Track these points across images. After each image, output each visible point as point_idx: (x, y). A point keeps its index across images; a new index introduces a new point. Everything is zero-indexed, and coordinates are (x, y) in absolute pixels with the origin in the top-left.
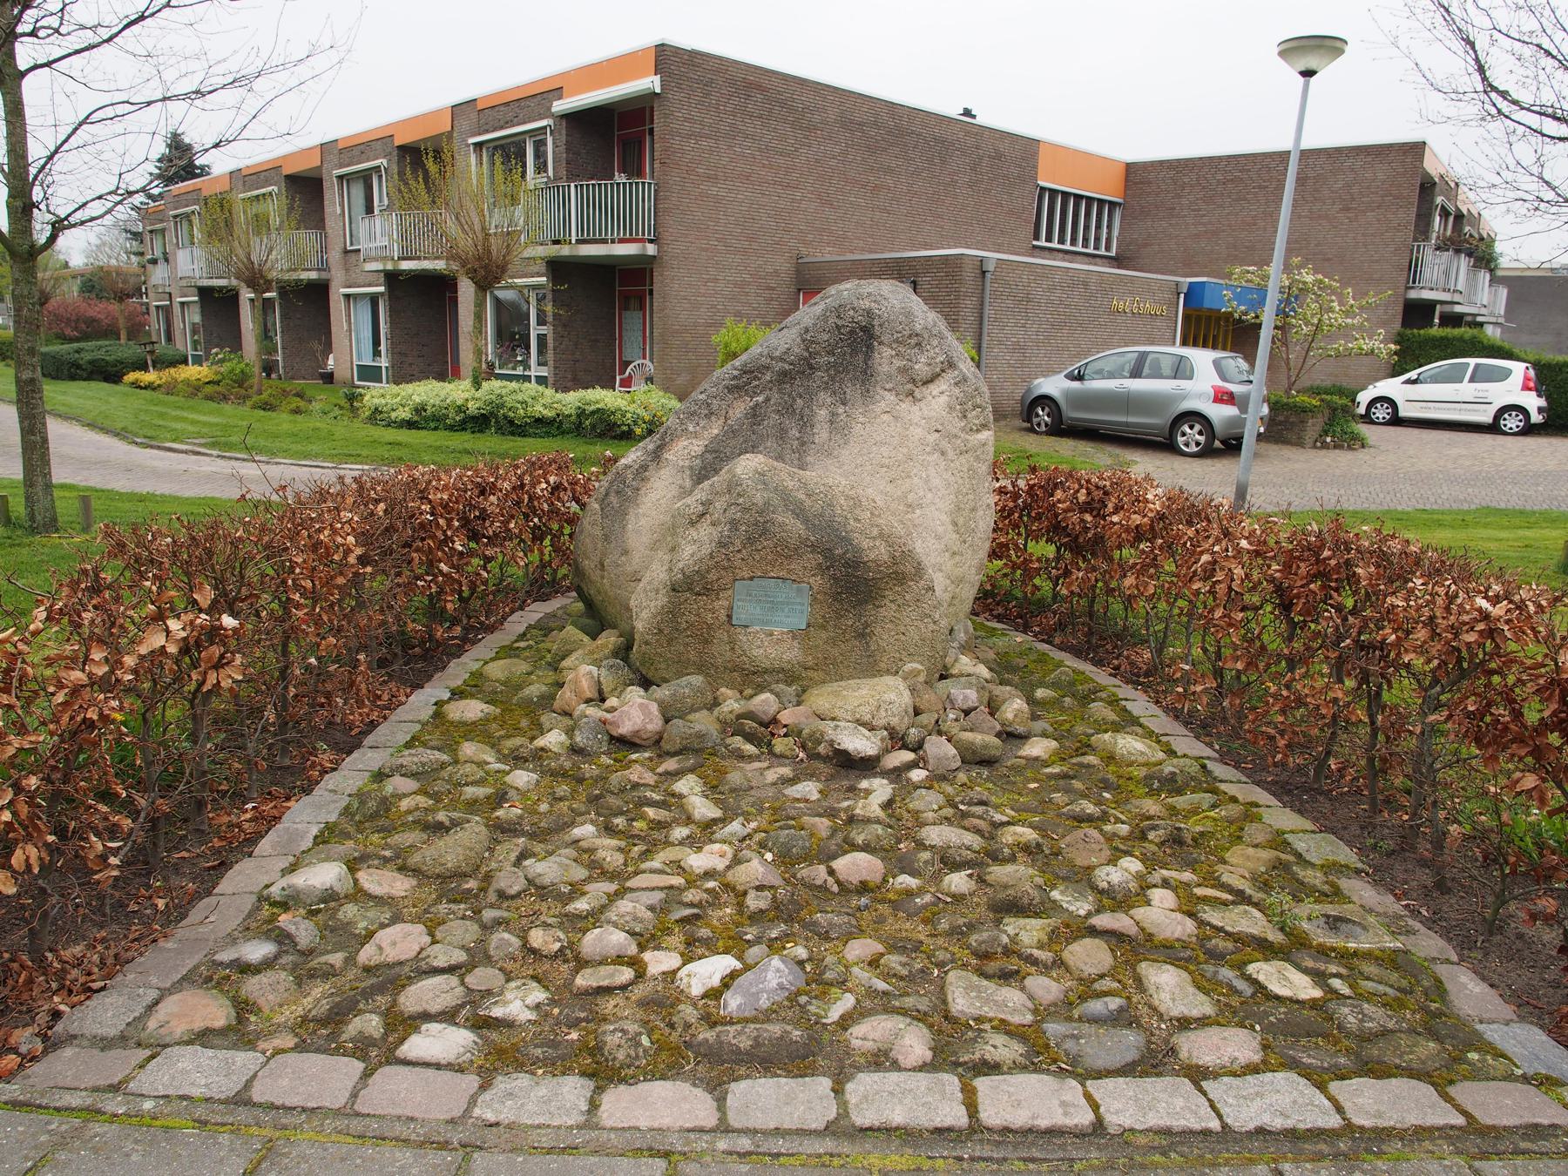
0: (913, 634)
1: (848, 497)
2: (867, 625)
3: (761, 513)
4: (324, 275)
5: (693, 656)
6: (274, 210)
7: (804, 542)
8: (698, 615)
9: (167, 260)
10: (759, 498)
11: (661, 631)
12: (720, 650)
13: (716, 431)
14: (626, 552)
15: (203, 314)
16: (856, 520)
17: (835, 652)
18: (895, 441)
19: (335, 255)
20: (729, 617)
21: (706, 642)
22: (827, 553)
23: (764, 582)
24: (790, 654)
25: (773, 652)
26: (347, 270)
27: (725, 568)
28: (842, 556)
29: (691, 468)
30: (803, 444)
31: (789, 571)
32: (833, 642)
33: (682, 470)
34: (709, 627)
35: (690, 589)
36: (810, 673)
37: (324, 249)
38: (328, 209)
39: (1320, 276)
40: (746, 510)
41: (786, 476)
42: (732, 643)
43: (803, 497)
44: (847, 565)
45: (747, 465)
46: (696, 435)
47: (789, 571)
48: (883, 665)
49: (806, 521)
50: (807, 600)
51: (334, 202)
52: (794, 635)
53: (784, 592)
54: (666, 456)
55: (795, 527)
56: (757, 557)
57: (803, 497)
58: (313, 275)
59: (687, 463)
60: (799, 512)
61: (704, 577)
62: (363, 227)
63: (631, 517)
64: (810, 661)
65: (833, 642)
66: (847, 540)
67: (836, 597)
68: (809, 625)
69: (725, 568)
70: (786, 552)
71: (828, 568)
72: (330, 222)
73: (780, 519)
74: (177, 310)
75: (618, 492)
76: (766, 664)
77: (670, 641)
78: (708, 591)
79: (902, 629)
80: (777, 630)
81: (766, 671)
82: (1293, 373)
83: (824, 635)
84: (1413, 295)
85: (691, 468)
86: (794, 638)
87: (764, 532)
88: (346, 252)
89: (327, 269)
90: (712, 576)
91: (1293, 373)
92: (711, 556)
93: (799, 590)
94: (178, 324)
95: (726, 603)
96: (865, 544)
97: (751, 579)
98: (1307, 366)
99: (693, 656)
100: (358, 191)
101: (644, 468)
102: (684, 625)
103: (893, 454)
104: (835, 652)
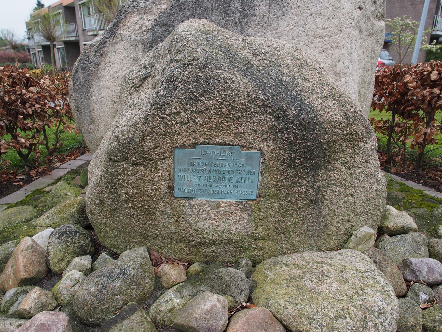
0: (361, 196)
1: (293, 58)
2: (319, 190)
3: (202, 68)
4: (77, 38)
5: (137, 226)
6: (61, 19)
7: (253, 100)
8: (137, 186)
9: (33, 38)
10: (201, 53)
11: (102, 202)
12: (164, 222)
13: (164, 7)
14: (93, 121)
15: (44, 54)
16: (306, 80)
17: (288, 221)
18: (329, 12)
19: (80, 32)
20: (171, 188)
21: (149, 214)
22: (279, 113)
23: (208, 149)
24: (239, 225)
25: (220, 225)
26: (84, 36)
27: (161, 134)
28: (296, 117)
29: (143, 41)
30: (245, 16)
31: (237, 135)
32: (285, 211)
33: (134, 43)
34: (151, 199)
35: (126, 159)
36: (261, 244)
37: (77, 31)
38: (77, 16)
39: (414, 21)
40: (185, 66)
41: (232, 38)
42: (176, 216)
43: (249, 56)
44: (302, 127)
45: (189, 27)
46: (146, 11)
47: (237, 135)
48: (332, 229)
49: (254, 79)
50: (257, 168)
51: (79, 14)
52: (243, 206)
53: (231, 159)
54: (120, 31)
55: (243, 85)
56: (199, 120)
57: (249, 56)
58: (74, 39)
59: (139, 37)
60: (246, 69)
61: (139, 145)
62: (87, 20)
63: (94, 90)
64: (261, 232)
65: (285, 211)
66: (298, 100)
67: (289, 163)
68: (259, 195)
69: (161, 134)
70: (234, 113)
71: (281, 131)
72: (78, 21)
73: (225, 75)
74: (37, 54)
75: (83, 69)
76: (214, 236)
77: (113, 212)
78: (145, 160)
79: (351, 191)
80: (224, 202)
81: (213, 243)
82: (402, 57)
83: (276, 205)
84: (434, 33)
85: (143, 41)
86: (243, 209)
87: (207, 90)
88: (83, 30)
89: (78, 36)
90: (148, 144)
91: (402, 57)
92: (146, 120)
93: (249, 158)
94: (38, 58)
95: (166, 174)
96: (318, 104)
97: (193, 145)
98: (407, 54)
99: (137, 226)
100: (86, 9)
101: (103, 44)
102: (124, 197)
103: (326, 25)
104: (288, 221)
